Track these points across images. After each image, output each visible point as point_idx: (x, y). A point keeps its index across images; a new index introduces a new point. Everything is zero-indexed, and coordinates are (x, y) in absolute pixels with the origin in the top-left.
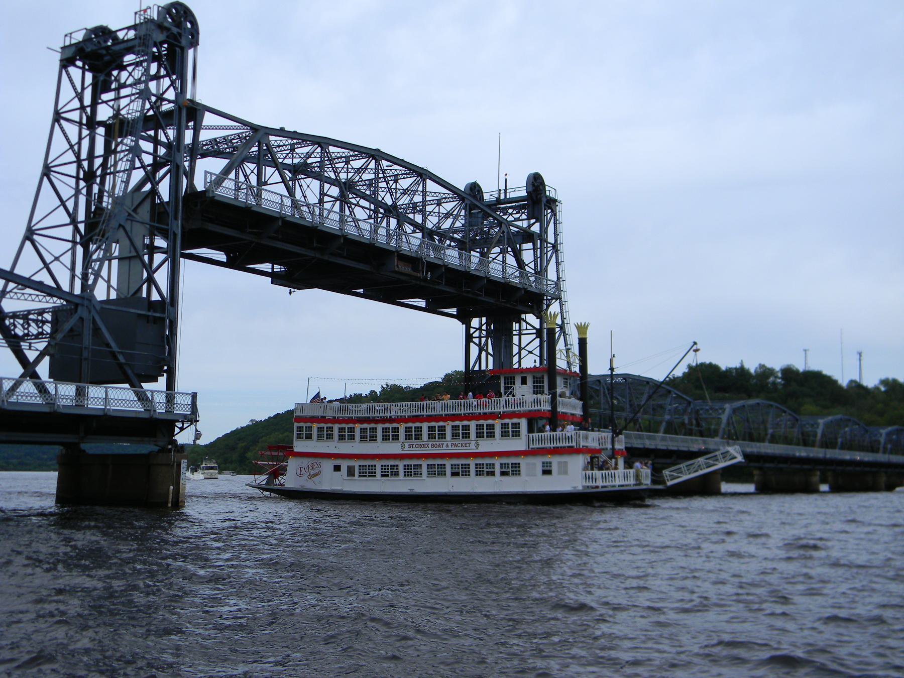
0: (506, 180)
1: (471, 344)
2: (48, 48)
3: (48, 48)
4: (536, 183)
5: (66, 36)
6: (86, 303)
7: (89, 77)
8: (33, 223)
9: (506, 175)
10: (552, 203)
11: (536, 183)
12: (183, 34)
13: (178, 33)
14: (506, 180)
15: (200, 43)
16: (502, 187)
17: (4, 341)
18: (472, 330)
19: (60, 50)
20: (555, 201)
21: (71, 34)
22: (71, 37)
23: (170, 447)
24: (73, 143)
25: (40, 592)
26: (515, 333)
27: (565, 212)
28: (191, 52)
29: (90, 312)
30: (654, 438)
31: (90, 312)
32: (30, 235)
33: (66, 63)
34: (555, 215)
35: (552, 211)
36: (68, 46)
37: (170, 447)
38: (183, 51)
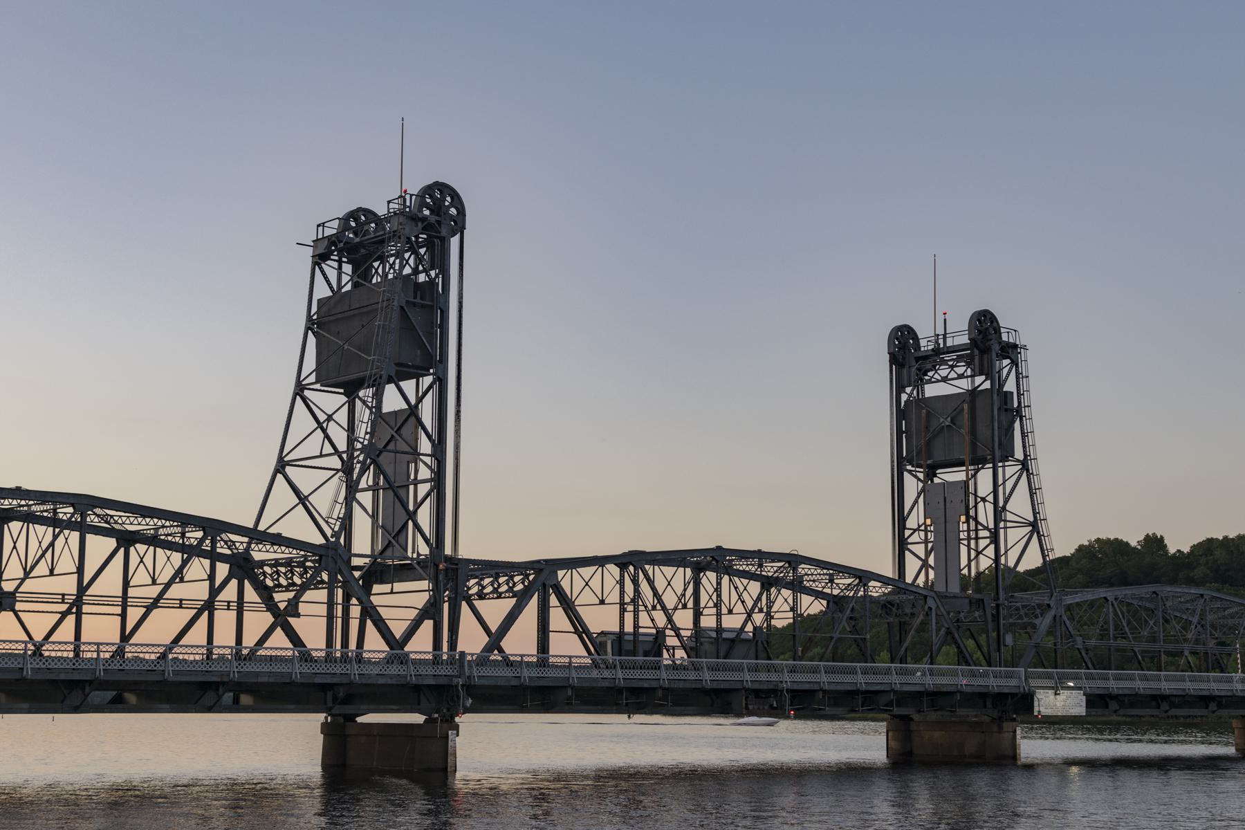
0: (945, 320)
1: (907, 552)
2: (297, 244)
3: (297, 244)
4: (984, 324)
5: (319, 226)
6: (331, 553)
7: (347, 268)
8: (285, 452)
9: (945, 314)
10: (1011, 351)
11: (984, 324)
12: (443, 221)
13: (437, 221)
14: (945, 320)
15: (466, 227)
16: (940, 331)
17: (263, 606)
18: (907, 533)
19: (312, 244)
20: (1015, 346)
21: (324, 223)
22: (323, 226)
23: (436, 716)
24: (74, 616)
25: (1179, 630)
26: (962, 536)
27: (1032, 361)
28: (455, 241)
29: (336, 563)
30: (1230, 681)
31: (336, 563)
32: (281, 466)
33: (320, 259)
34: (1017, 366)
35: (1012, 362)
36: (320, 239)
37: (436, 716)
38: (444, 243)
